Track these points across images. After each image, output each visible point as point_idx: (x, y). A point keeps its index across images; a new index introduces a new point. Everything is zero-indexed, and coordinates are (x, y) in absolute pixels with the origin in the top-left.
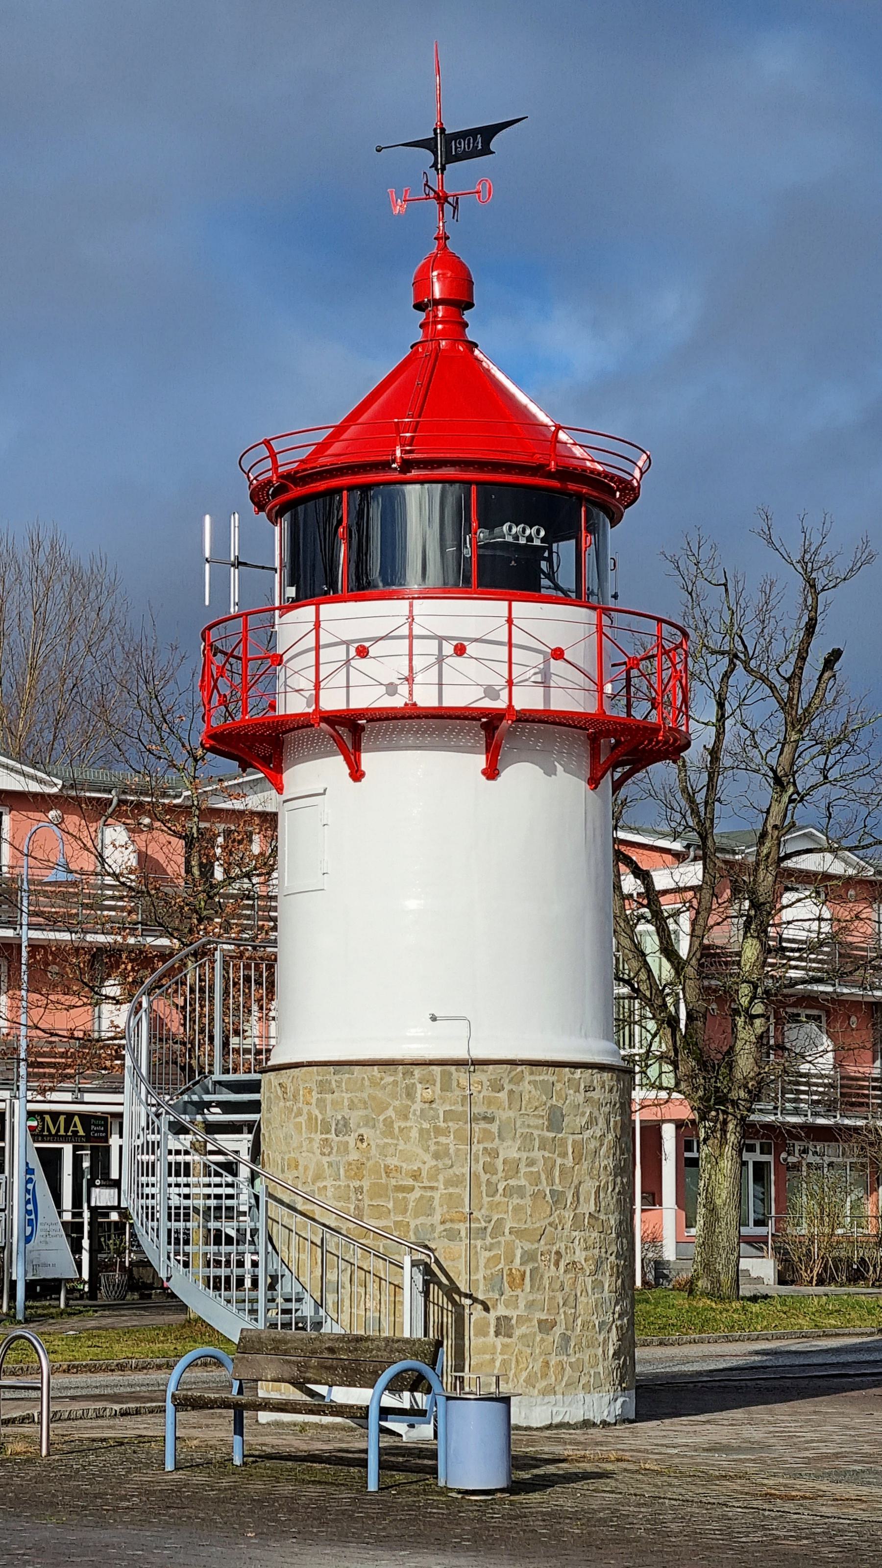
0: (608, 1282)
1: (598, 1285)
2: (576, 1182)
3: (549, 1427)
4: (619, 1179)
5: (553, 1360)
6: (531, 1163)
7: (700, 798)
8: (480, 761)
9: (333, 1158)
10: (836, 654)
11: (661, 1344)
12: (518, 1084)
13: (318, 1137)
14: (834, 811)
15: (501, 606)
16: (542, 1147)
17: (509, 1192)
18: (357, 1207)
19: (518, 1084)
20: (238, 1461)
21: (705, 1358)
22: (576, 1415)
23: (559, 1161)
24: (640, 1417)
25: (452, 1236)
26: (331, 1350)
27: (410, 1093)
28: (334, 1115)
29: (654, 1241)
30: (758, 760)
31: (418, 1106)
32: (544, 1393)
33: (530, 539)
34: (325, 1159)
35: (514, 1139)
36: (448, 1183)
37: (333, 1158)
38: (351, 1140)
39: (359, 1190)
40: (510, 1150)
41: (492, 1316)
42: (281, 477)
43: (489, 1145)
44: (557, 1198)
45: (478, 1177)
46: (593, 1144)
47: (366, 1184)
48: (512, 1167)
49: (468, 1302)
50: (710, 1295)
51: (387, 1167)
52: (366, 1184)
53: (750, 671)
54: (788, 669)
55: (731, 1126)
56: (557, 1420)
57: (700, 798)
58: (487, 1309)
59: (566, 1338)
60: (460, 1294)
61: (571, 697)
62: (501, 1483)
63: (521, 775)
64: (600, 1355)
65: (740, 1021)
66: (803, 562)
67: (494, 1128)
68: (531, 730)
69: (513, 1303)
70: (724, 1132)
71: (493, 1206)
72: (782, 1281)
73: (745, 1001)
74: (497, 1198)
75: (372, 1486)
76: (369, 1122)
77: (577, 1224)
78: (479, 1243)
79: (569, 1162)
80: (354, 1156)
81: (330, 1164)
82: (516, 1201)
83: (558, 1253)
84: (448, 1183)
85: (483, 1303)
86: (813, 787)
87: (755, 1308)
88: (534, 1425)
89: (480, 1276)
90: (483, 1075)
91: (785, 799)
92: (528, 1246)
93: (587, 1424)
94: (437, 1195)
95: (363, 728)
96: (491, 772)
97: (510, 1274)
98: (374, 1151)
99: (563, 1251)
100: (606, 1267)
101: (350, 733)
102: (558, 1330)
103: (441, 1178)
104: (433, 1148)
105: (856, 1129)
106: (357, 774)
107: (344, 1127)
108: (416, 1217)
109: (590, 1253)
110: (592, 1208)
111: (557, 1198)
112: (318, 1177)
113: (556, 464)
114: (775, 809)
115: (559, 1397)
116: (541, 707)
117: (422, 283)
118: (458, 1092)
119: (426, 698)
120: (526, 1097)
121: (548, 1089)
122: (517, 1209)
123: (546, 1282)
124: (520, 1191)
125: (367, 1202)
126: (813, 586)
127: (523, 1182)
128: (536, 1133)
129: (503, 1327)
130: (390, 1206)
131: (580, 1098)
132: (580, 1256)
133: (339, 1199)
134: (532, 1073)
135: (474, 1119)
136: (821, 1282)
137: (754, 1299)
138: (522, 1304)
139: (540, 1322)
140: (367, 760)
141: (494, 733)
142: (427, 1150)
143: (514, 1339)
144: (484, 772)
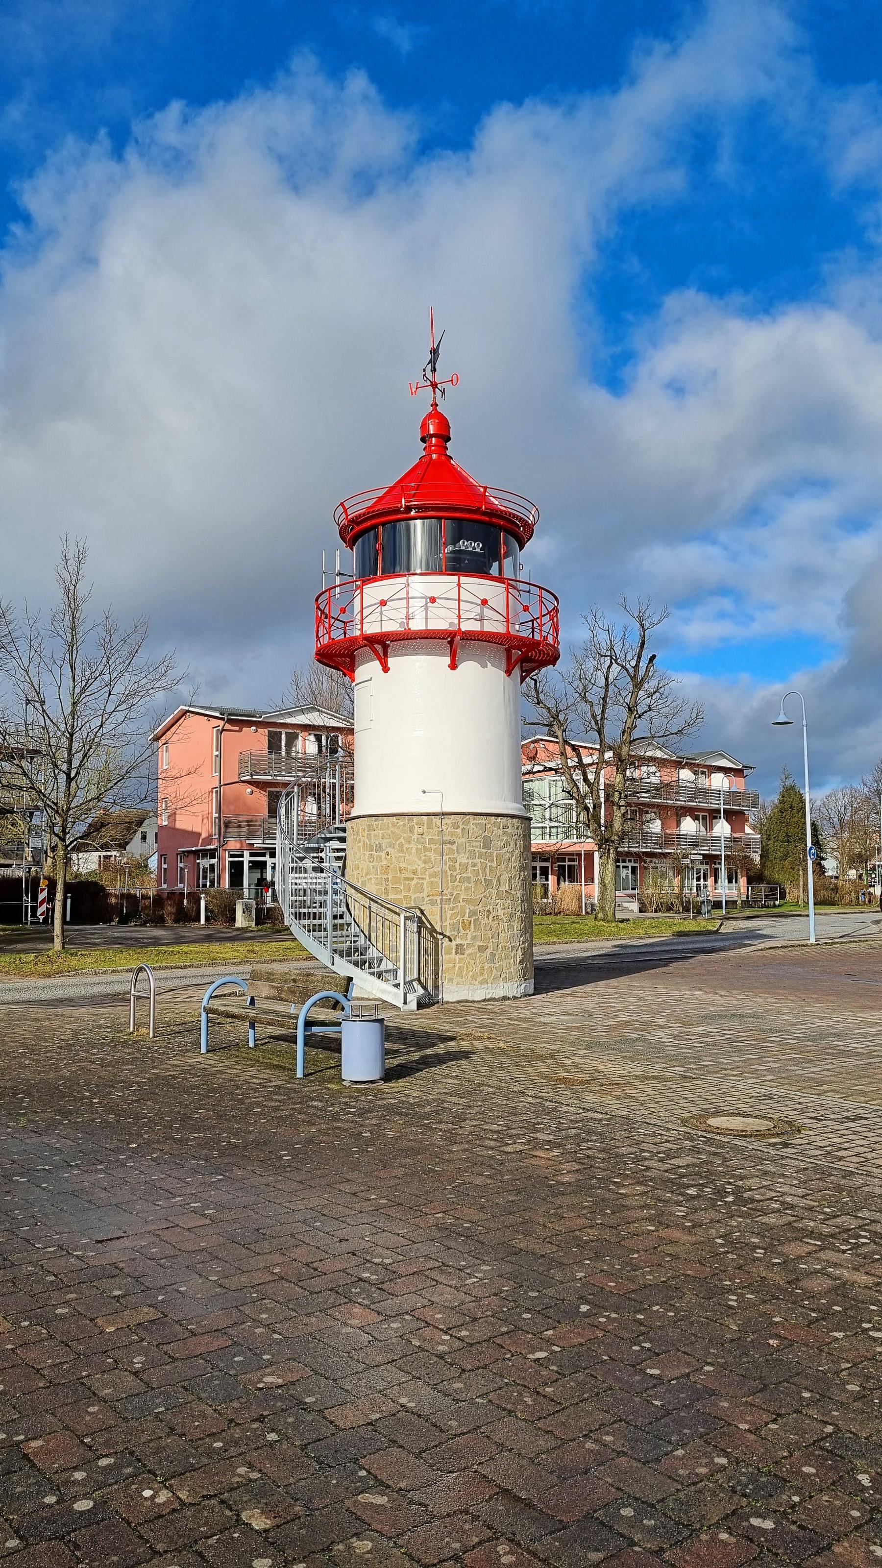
0: (517, 926)
1: (511, 927)
2: (498, 875)
3: (484, 1000)
4: (522, 873)
5: (486, 966)
6: (474, 865)
7: (599, 718)
8: (447, 660)
9: (374, 864)
10: (654, 657)
11: (578, 942)
12: (467, 825)
13: (367, 853)
14: (653, 721)
15: (455, 579)
16: (480, 857)
17: (463, 880)
18: (386, 888)
19: (467, 825)
20: (251, 1044)
21: (594, 949)
22: (499, 994)
23: (489, 864)
24: (537, 991)
25: (433, 903)
26: (294, 981)
27: (411, 831)
28: (375, 842)
29: (589, 896)
30: (621, 701)
31: (415, 836)
32: (481, 983)
33: (474, 548)
34: (371, 864)
35: (465, 853)
36: (431, 876)
37: (374, 864)
38: (383, 854)
39: (387, 880)
40: (463, 859)
41: (454, 943)
42: (349, 521)
43: (452, 856)
44: (488, 883)
45: (446, 872)
46: (508, 855)
47: (390, 877)
48: (464, 868)
49: (441, 937)
50: (603, 920)
51: (400, 868)
52: (390, 877)
53: (618, 664)
54: (633, 663)
55: (611, 851)
56: (488, 997)
57: (599, 718)
58: (450, 940)
59: (493, 955)
60: (437, 933)
61: (494, 625)
62: (376, 1076)
63: (468, 667)
64: (512, 962)
65: (615, 808)
66: (639, 617)
67: (454, 847)
68: (474, 645)
69: (465, 937)
70: (609, 853)
71: (453, 888)
72: (641, 911)
73: (616, 800)
74: (456, 883)
75: (299, 1074)
76: (392, 845)
77: (499, 896)
78: (447, 906)
79: (495, 864)
80: (384, 862)
81: (373, 867)
82: (466, 884)
83: (488, 911)
84: (431, 876)
85: (449, 937)
86: (646, 712)
87: (622, 925)
88: (476, 999)
89: (447, 923)
90: (448, 821)
91: (633, 717)
92: (472, 908)
93: (505, 998)
94: (425, 882)
95: (389, 645)
96: (453, 666)
97: (463, 922)
98: (394, 860)
99: (491, 910)
100: (515, 918)
101: (382, 646)
102: (489, 951)
103: (427, 873)
104: (423, 858)
105: (669, 853)
106: (386, 669)
107: (379, 848)
108: (415, 893)
109: (506, 911)
110: (507, 888)
111: (488, 883)
112: (368, 874)
113: (486, 508)
114: (629, 721)
115: (490, 985)
116: (479, 629)
117: (424, 426)
118: (436, 829)
119: (417, 625)
120: (471, 831)
121: (484, 828)
122: (467, 889)
123: (482, 926)
124: (468, 879)
125: (391, 886)
126: (643, 627)
127: (470, 875)
128: (477, 850)
129: (460, 949)
130: (402, 888)
131: (501, 832)
132: (501, 912)
133: (377, 884)
134: (474, 819)
135: (443, 843)
136: (656, 911)
137: (622, 921)
138: (469, 937)
139: (479, 946)
140: (391, 661)
141: (454, 644)
142: (420, 859)
143: (465, 956)
144: (449, 666)
